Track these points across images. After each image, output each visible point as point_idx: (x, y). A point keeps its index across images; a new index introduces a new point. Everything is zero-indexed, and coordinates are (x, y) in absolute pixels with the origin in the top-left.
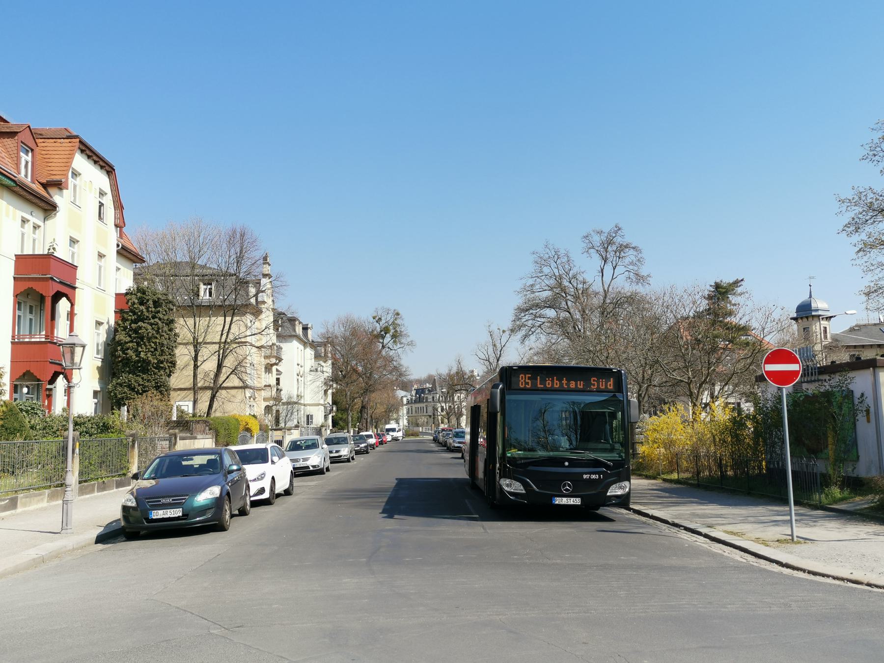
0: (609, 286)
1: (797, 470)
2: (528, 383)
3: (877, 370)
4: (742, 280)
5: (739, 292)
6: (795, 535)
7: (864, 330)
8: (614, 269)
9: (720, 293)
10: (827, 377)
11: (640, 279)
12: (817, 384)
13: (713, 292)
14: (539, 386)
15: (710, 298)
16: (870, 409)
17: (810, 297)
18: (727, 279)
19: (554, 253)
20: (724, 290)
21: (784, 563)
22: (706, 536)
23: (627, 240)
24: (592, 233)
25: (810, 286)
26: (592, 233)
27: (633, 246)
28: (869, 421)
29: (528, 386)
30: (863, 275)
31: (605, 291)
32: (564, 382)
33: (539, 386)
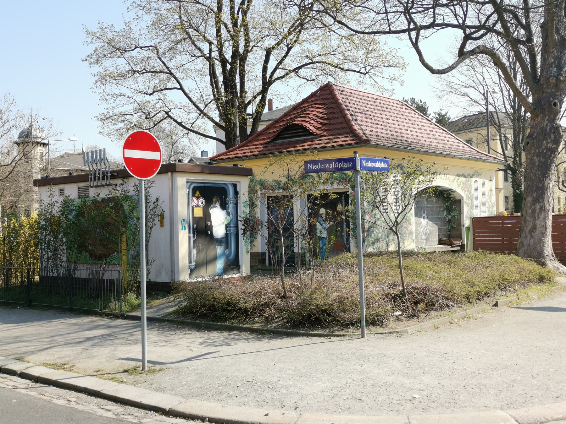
1: (88, 277)
3: (175, 175)
6: (147, 358)
7: (71, 158)
10: (119, 181)
12: (110, 188)
16: (165, 213)
21: (167, 410)
22: (23, 376)
28: (162, 225)
30: (100, 102)
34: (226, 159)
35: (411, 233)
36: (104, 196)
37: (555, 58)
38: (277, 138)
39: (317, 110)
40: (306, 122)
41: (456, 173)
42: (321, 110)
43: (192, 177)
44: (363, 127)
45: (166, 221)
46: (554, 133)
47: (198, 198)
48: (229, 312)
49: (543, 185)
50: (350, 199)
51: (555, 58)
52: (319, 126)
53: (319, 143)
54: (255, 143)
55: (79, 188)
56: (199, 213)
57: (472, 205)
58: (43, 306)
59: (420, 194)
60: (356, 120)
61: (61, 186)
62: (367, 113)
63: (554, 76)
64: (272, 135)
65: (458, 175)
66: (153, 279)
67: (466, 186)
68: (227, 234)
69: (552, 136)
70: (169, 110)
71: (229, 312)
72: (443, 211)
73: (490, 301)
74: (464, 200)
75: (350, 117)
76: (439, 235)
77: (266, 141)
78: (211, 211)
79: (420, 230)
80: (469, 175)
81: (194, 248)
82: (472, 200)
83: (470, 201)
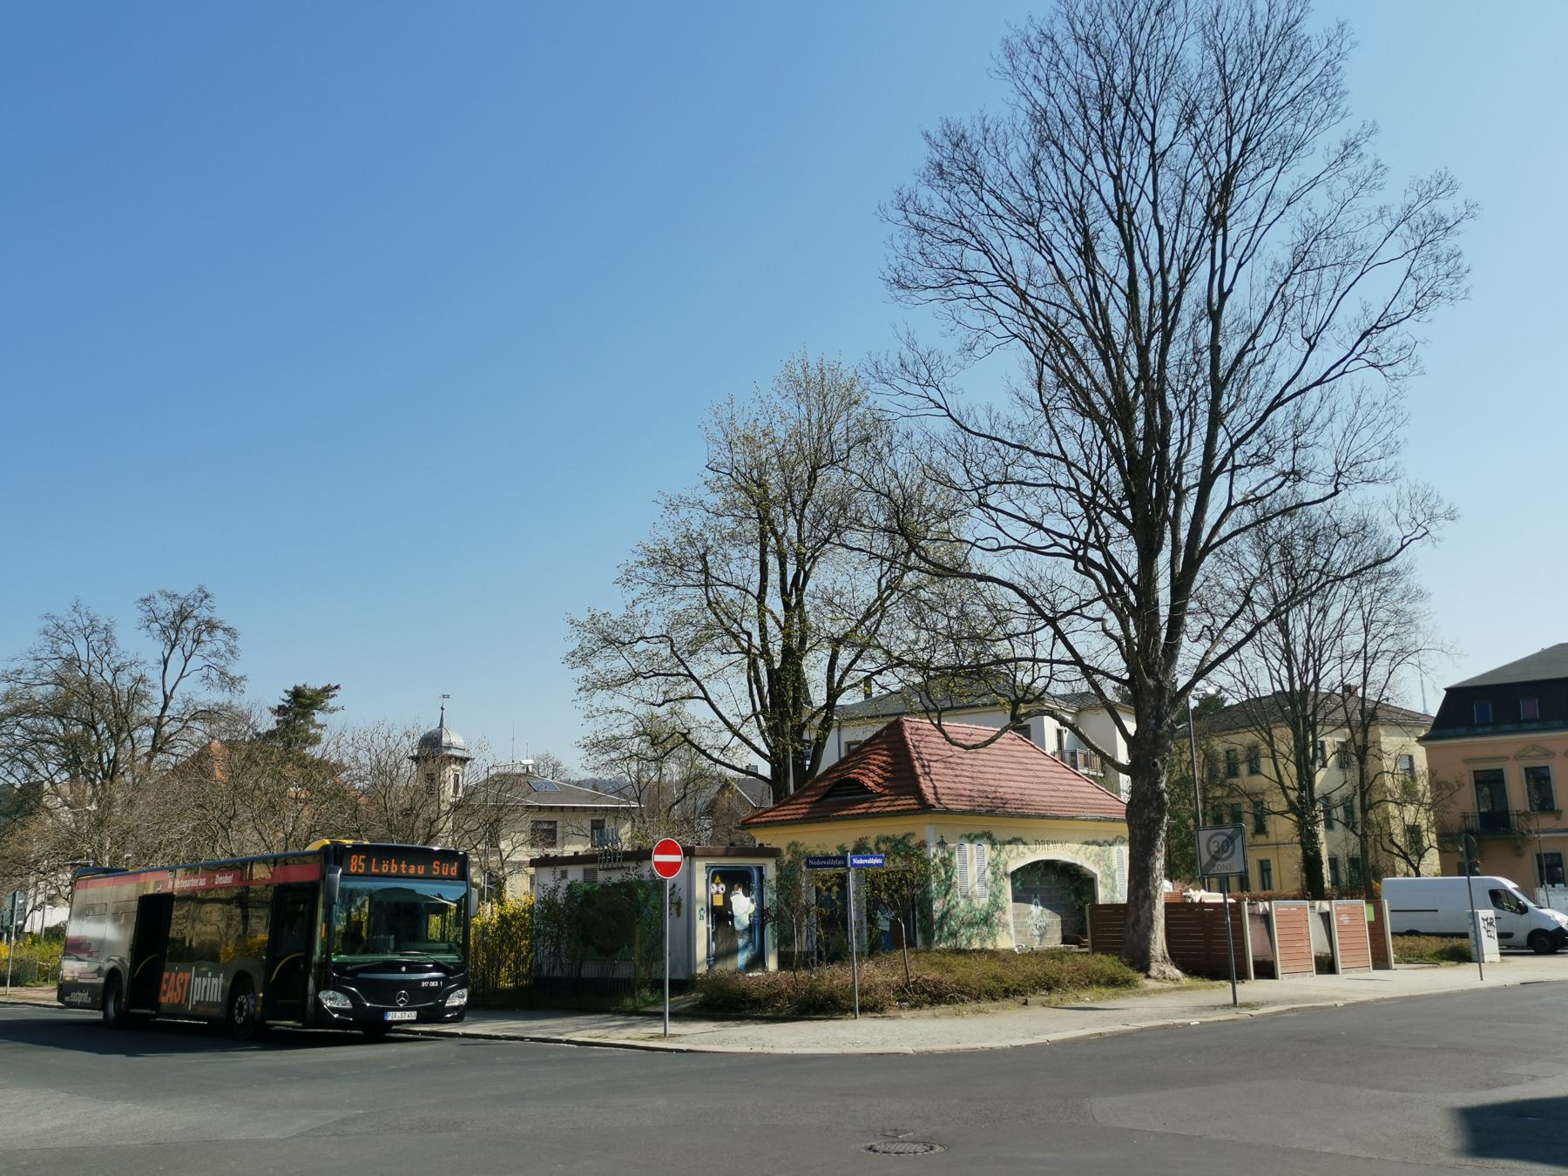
0: (174, 688)
2: (359, 867)
3: (693, 859)
4: (337, 687)
5: (330, 706)
8: (186, 661)
9: (301, 706)
10: (633, 864)
11: (232, 683)
13: (288, 701)
14: (373, 870)
15: (281, 710)
17: (441, 725)
18: (315, 683)
19: (87, 623)
20: (308, 701)
23: (217, 616)
24: (158, 596)
25: (442, 709)
26: (158, 596)
27: (225, 626)
29: (361, 871)
30: (584, 721)
31: (166, 696)
32: (403, 866)
33: (373, 870)
34: (762, 822)
35: (1005, 925)
36: (616, 881)
37: (1153, 708)
38: (828, 795)
39: (880, 757)
40: (864, 775)
41: (1083, 840)
42: (885, 758)
43: (712, 861)
44: (937, 784)
45: (684, 910)
46: (1157, 799)
47: (718, 884)
48: (744, 1003)
49: (1147, 866)
51: (1153, 708)
52: (881, 781)
53: (879, 806)
54: (800, 801)
55: (585, 871)
56: (719, 902)
60: (928, 774)
61: (564, 868)
62: (950, 759)
63: (1152, 730)
64: (822, 790)
65: (1086, 843)
66: (674, 977)
67: (1099, 859)
69: (1155, 804)
70: (686, 731)
71: (744, 1003)
72: (1069, 895)
73: (1021, 999)
74: (1099, 878)
75: (919, 770)
76: (1062, 930)
77: (814, 799)
78: (732, 899)
79: (1029, 922)
80: (1105, 842)
81: (713, 940)
82: (1113, 878)
83: (1110, 880)
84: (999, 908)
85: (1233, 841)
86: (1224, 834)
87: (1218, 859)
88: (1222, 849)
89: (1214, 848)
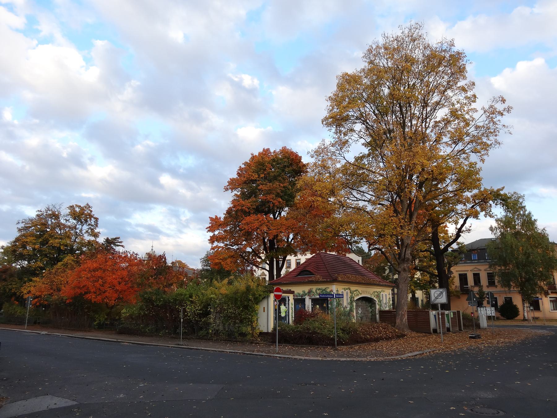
50: (329, 302)
57: (381, 305)
58: (551, 327)
59: (358, 300)
64: (296, 273)
68: (285, 315)
82: (381, 303)
84: (352, 311)
85: (442, 293)
86: (440, 291)
87: (437, 299)
88: (439, 295)
89: (436, 295)
